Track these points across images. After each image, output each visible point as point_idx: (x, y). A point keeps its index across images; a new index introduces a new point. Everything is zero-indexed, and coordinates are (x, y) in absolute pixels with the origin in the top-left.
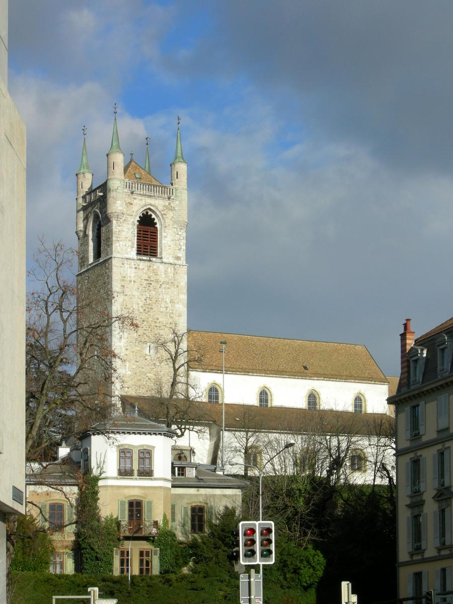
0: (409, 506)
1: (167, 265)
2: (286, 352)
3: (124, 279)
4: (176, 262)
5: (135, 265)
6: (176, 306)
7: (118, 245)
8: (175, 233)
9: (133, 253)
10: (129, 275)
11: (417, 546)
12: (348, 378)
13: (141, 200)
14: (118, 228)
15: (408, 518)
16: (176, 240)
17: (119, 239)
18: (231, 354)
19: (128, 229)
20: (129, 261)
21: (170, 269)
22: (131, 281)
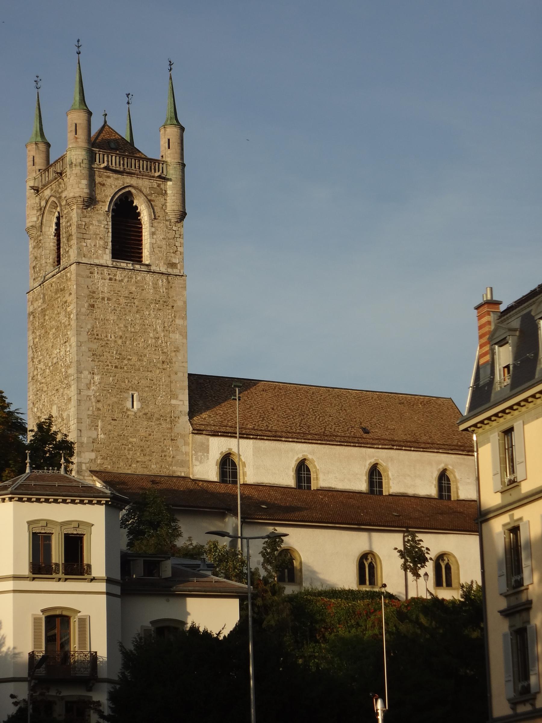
0: (506, 613)
1: (157, 275)
2: (336, 407)
3: (94, 295)
4: (170, 271)
5: (109, 274)
6: (171, 335)
7: (85, 244)
8: (167, 227)
9: (106, 258)
10: (101, 289)
11: (523, 687)
12: (428, 446)
13: (117, 179)
14: (84, 219)
15: (505, 635)
16: (169, 239)
17: (86, 236)
18: (255, 410)
19: (99, 221)
20: (101, 269)
21: (162, 282)
22: (103, 299)
